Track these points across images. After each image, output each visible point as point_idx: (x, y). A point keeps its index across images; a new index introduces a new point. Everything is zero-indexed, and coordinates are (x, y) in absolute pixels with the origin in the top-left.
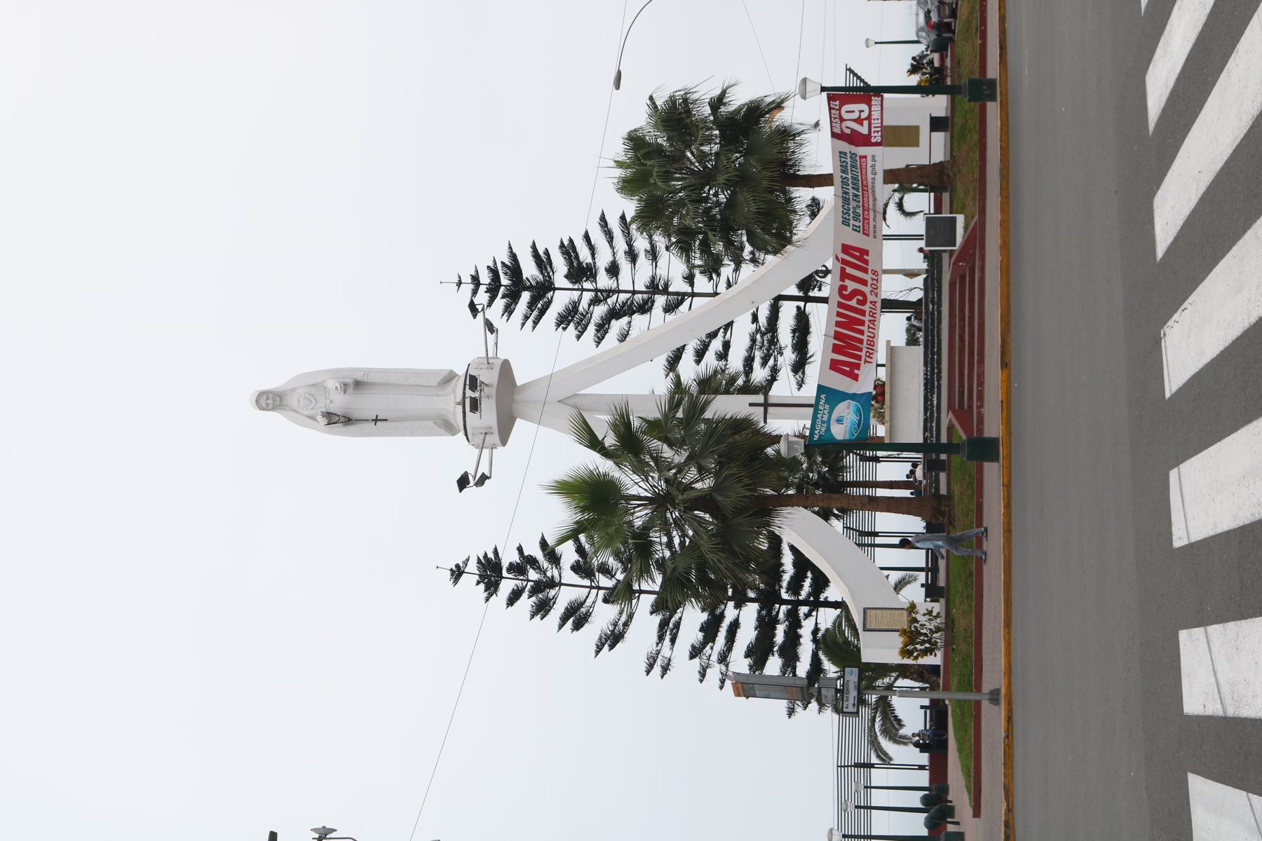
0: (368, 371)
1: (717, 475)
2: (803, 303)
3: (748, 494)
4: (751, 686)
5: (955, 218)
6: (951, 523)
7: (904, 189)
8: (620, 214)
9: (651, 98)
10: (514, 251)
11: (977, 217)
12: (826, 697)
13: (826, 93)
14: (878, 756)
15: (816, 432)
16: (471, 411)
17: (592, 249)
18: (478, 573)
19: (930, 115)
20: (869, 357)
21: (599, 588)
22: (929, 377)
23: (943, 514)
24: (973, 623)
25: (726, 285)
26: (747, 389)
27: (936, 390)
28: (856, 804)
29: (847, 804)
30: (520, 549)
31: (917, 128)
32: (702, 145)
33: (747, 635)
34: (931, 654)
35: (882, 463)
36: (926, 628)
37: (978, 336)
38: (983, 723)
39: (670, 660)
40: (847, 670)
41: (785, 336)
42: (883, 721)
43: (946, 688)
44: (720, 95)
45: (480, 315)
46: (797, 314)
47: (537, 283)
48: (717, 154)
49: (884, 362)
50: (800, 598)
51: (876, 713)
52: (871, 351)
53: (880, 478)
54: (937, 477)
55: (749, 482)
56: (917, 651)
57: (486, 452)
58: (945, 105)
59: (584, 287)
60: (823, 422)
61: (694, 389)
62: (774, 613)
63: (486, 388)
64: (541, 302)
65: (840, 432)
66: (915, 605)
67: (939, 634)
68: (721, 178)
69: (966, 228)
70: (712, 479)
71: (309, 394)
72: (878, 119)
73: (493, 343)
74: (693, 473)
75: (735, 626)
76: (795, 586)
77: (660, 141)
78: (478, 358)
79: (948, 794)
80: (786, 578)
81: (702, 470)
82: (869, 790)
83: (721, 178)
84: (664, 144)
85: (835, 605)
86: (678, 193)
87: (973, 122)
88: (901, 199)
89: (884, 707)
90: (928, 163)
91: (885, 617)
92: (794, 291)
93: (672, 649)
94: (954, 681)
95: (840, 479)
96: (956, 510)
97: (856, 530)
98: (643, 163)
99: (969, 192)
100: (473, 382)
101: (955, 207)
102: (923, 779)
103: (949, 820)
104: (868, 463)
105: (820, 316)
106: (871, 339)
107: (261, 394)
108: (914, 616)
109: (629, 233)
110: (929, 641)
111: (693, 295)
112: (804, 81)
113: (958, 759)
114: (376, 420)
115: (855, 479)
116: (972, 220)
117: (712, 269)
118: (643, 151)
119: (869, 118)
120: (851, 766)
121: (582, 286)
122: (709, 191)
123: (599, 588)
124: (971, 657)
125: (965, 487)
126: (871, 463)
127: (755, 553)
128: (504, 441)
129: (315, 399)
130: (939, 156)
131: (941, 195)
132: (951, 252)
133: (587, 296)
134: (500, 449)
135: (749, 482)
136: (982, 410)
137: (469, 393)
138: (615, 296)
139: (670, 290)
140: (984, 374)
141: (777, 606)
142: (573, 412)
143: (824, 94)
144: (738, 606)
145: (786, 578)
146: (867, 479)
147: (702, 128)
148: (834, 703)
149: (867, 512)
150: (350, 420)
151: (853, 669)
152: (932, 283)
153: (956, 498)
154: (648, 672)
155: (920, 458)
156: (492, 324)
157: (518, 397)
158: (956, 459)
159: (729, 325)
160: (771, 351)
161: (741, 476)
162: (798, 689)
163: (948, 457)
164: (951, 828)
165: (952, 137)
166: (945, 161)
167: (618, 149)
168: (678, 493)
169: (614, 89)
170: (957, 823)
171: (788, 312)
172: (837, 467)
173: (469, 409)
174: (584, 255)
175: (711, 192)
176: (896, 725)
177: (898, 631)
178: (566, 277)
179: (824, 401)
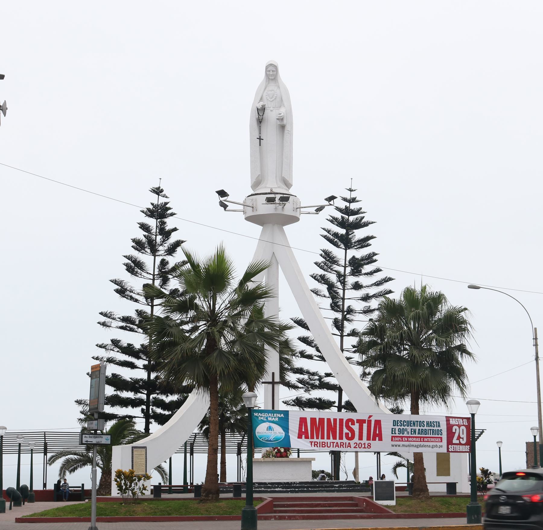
0: (291, 134)
1: (230, 353)
2: (337, 406)
3: (218, 372)
4: (98, 376)
5: (393, 500)
6: (201, 501)
7: (410, 467)
8: (392, 290)
9: (466, 309)
10: (370, 225)
11: (394, 513)
12: (92, 424)
13: (471, 417)
14: (53, 457)
15: (260, 414)
16: (267, 198)
17: (371, 273)
18: (159, 204)
19: (457, 483)
20: (315, 445)
21: (154, 280)
22: (293, 485)
23: (207, 496)
24: (138, 516)
25: (348, 357)
26: (283, 370)
27: (285, 490)
28: (21, 444)
29: (22, 438)
30: (175, 229)
31: (448, 474)
32: (436, 340)
33: (127, 374)
34: (118, 490)
35: (237, 457)
36: (135, 486)
37: (320, 516)
38: (75, 523)
39: (109, 326)
40: (109, 437)
41: (317, 394)
42: (75, 460)
43: (98, 500)
44: (467, 351)
45: (327, 203)
46: (330, 401)
47: (350, 239)
48: (431, 349)
49: (300, 457)
50: (145, 408)
51: (80, 456)
52: (318, 445)
53: (227, 456)
54: (230, 492)
55: (226, 374)
56: (120, 481)
57: (241, 207)
58: (463, 492)
59: (347, 268)
60: (267, 418)
61: (283, 339)
62: (141, 390)
63: (281, 207)
64: (338, 241)
65: (261, 430)
66: (149, 479)
67: (131, 495)
68: (415, 353)
69: (387, 506)
70: (227, 349)
71: (276, 97)
72: (459, 449)
73: (309, 211)
74: (230, 337)
75: (132, 366)
76: (160, 404)
77: (438, 314)
78: (300, 202)
79: (28, 502)
80: (163, 397)
81: (233, 342)
82: (30, 452)
83: (415, 353)
84: (437, 316)
85: (147, 429)
86: (406, 326)
87: (454, 509)
88: (403, 465)
89: (85, 461)
90: (427, 482)
91: (141, 460)
92: (345, 399)
93: (117, 327)
94: (102, 505)
95: (226, 430)
96: (209, 504)
97: (194, 441)
98: (424, 304)
99: (410, 508)
100: (285, 199)
101: (400, 499)
102: (38, 486)
103: (13, 503)
104: (237, 448)
105: (332, 413)
106: (326, 444)
107: (276, 67)
108: (143, 478)
109: (380, 296)
110: (126, 489)
111: (342, 336)
112: (478, 403)
113: (51, 508)
114: (260, 139)
115: (226, 440)
116: (392, 510)
117: (360, 348)
118: (432, 303)
119: (460, 444)
120: (45, 441)
121: (347, 267)
122: (408, 345)
123: (154, 280)
124: (117, 515)
125: (224, 509)
126: (237, 450)
127: (181, 377)
128: (248, 219)
129: (273, 101)
130: (432, 489)
131: (407, 491)
132: (372, 498)
133: (341, 269)
134: (243, 217)
135: (226, 374)
136: (273, 519)
137: (278, 197)
138: (341, 287)
139: (345, 321)
140: (295, 520)
141: (146, 392)
142: (267, 263)
143: (470, 416)
144: (145, 367)
145: (163, 397)
146: (226, 448)
147: (447, 340)
148: (88, 429)
149: (207, 448)
150: (260, 122)
151: (110, 441)
152: (353, 486)
153: (217, 504)
154: (101, 314)
155: (240, 481)
156: (321, 210)
157: (276, 227)
158: (242, 504)
159: (323, 359)
160: (307, 385)
161: (230, 369)
162: (97, 406)
163: (243, 499)
164: (8, 504)
165: (443, 496)
166: (428, 492)
167: (433, 289)
168: (218, 329)
169: (469, 284)
170: (10, 508)
171: (331, 396)
172: (233, 428)
173: (268, 197)
174: (367, 268)
175: (407, 346)
176: (71, 468)
177: (132, 469)
178: (354, 257)
179: (279, 416)
